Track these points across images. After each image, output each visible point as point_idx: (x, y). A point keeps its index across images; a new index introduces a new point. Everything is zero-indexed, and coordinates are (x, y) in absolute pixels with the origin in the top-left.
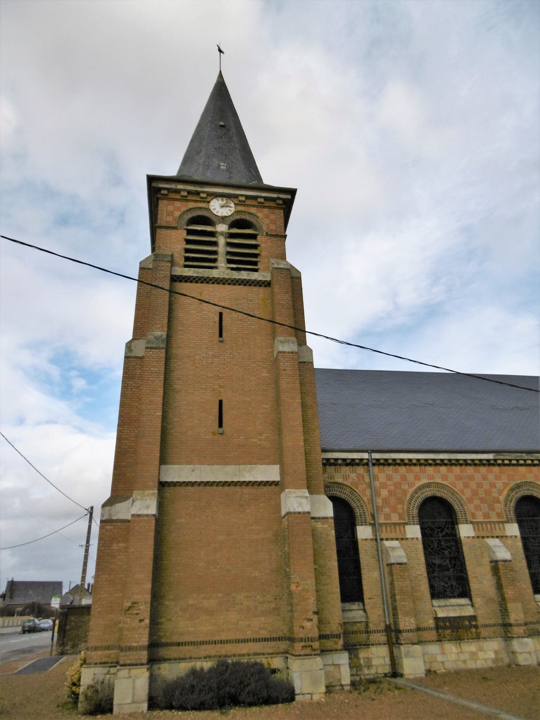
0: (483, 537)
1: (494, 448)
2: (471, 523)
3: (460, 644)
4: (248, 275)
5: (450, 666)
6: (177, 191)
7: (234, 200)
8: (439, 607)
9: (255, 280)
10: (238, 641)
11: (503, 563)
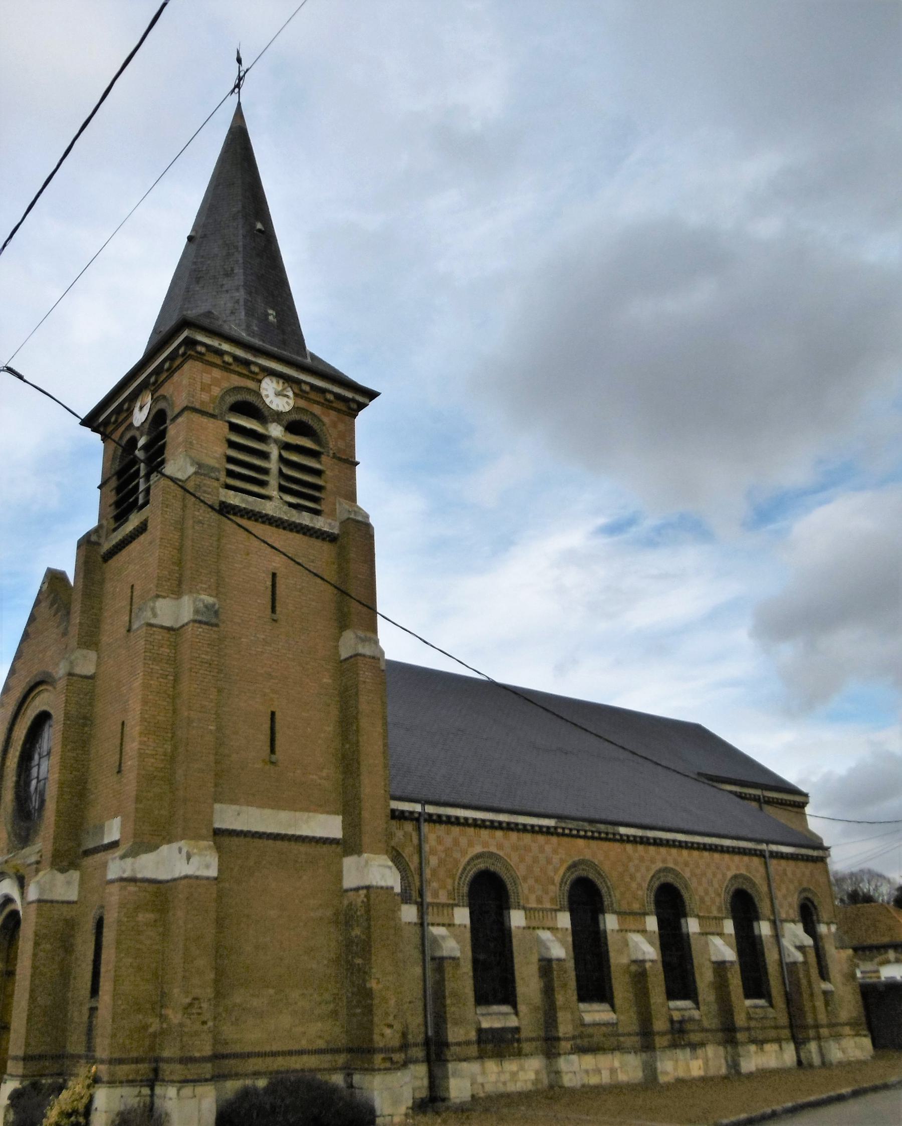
0: (534, 928)
1: (559, 811)
2: (524, 908)
3: (501, 1061)
4: (312, 520)
5: (489, 1088)
6: (220, 353)
7: (294, 386)
8: (483, 1015)
9: (319, 530)
10: (290, 1053)
11: (557, 962)
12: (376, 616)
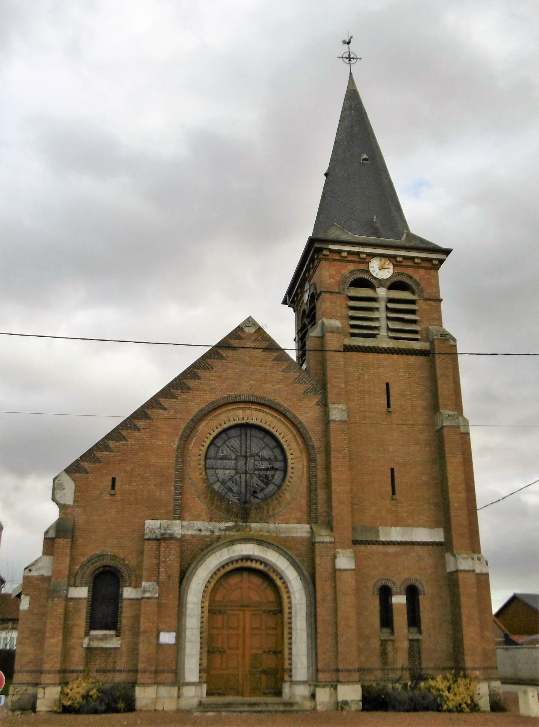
12: (285, 352)
